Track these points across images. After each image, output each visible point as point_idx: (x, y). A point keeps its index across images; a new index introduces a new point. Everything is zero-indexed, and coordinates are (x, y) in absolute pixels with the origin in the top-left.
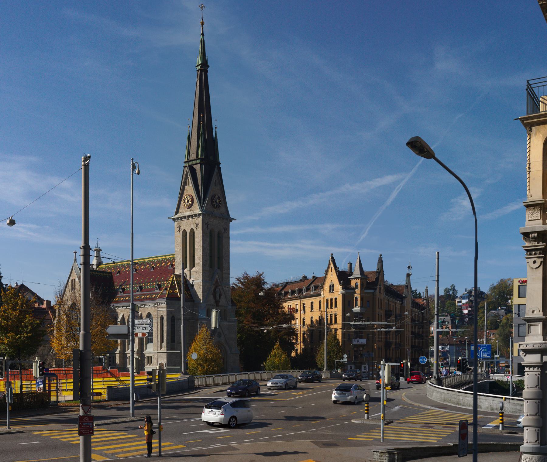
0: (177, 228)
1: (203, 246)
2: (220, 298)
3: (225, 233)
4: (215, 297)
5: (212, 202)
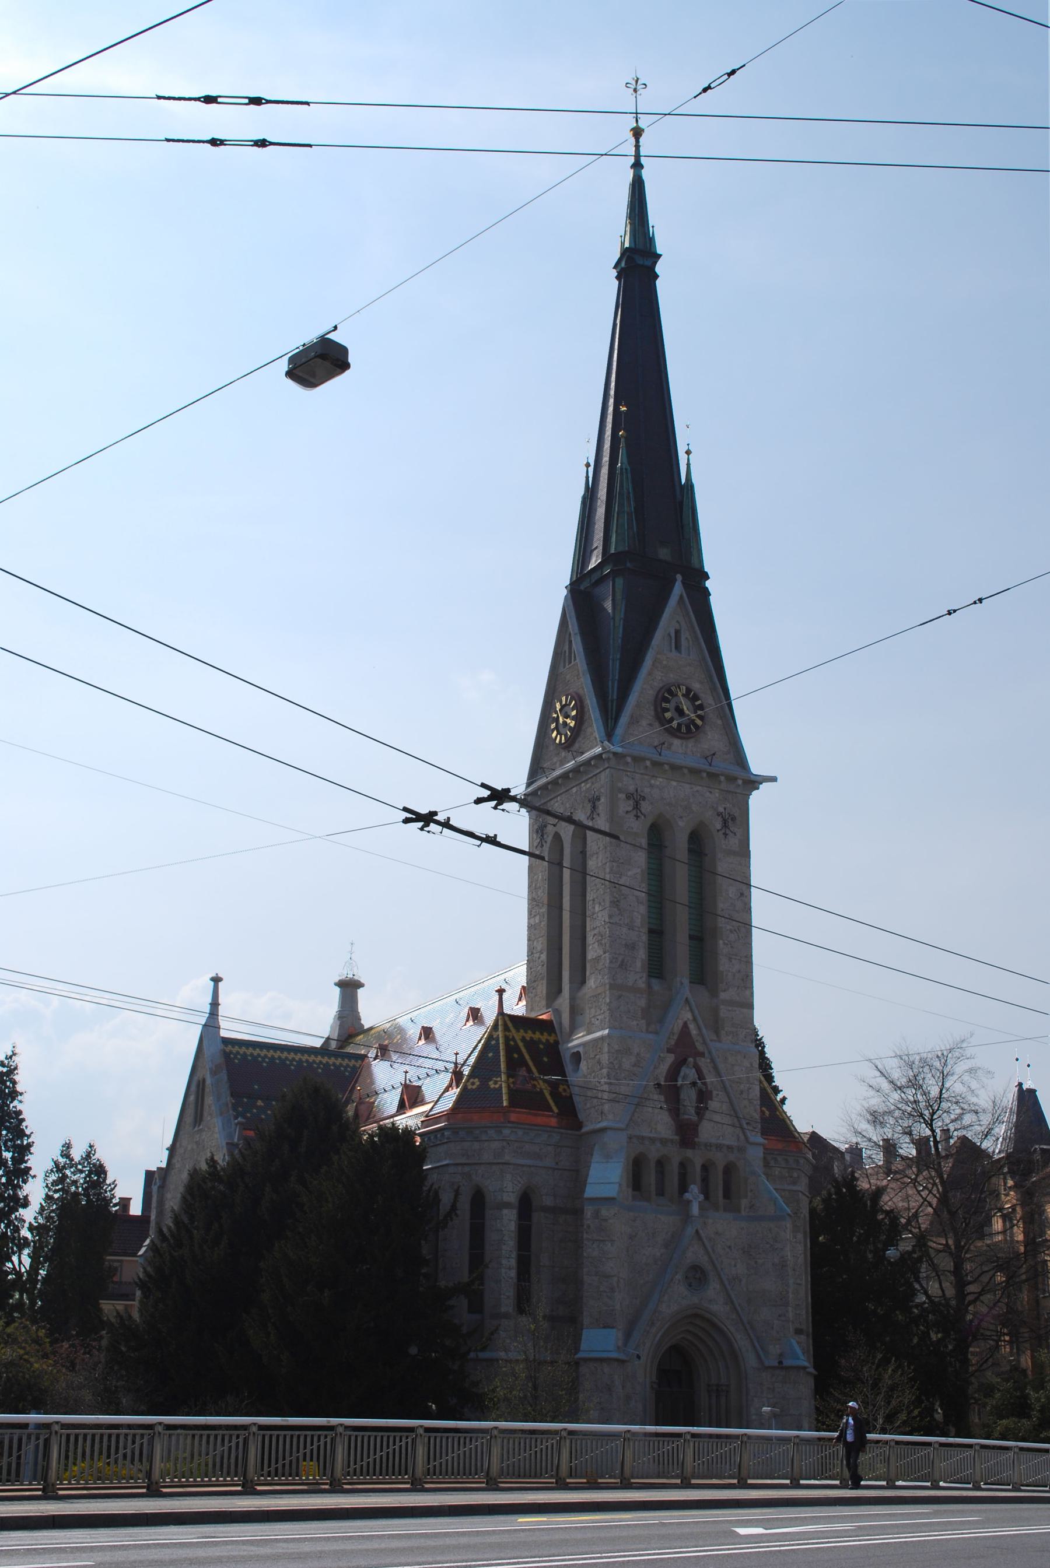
2: (700, 1112)
3: (725, 834)
4: (674, 1106)
5: (659, 710)
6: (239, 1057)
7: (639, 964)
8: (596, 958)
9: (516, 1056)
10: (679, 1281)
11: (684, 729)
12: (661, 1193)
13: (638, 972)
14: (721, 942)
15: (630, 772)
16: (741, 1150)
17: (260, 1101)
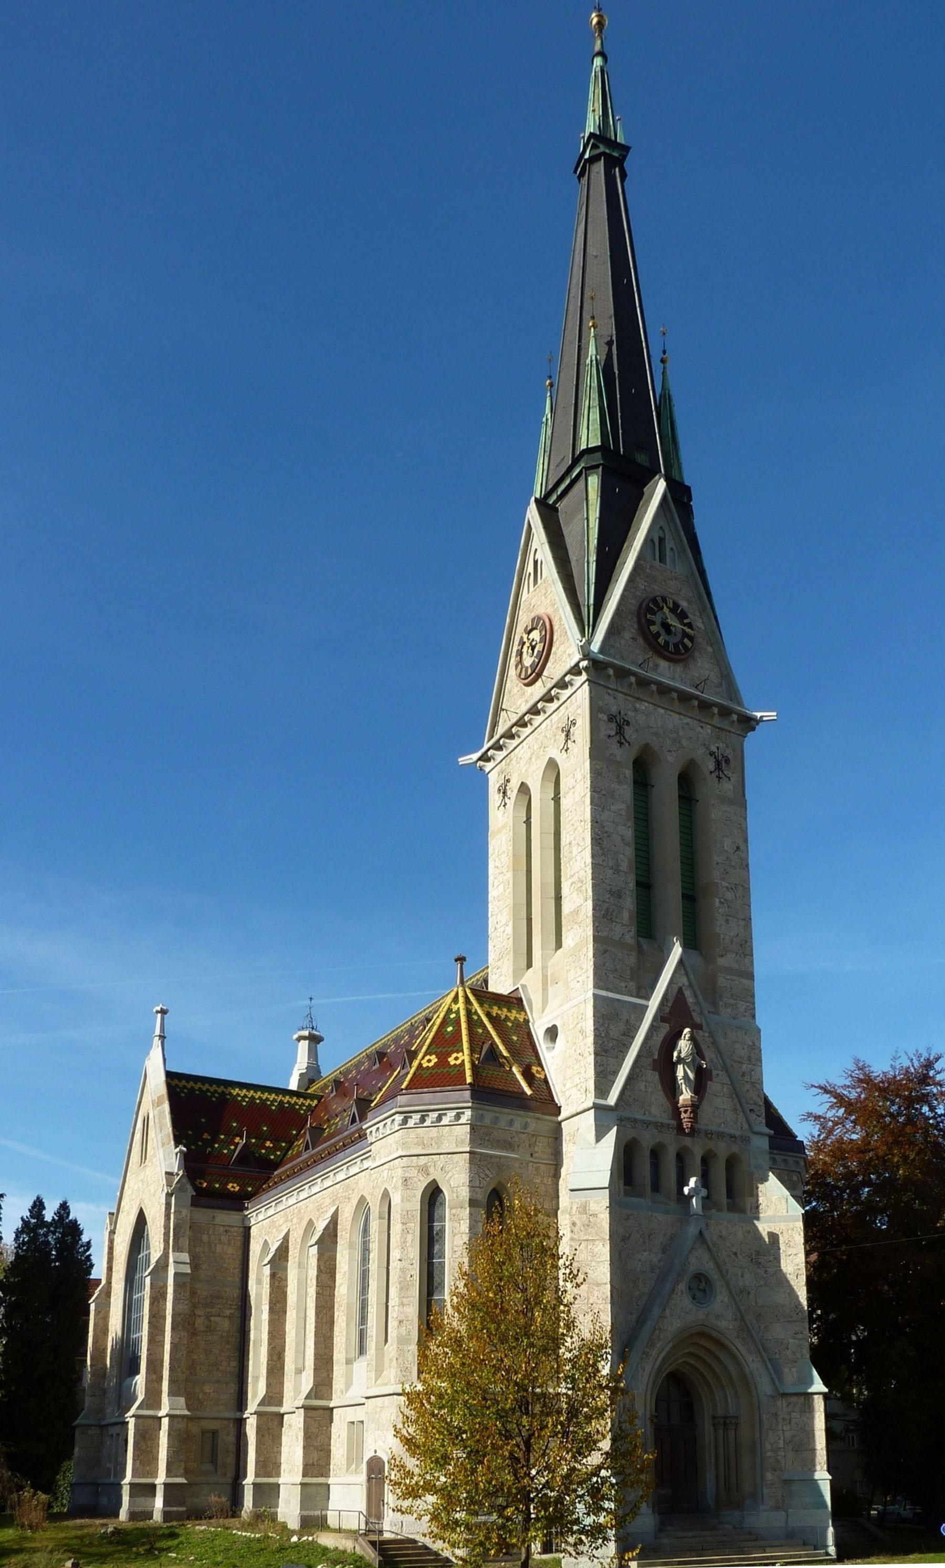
1: (595, 822)
5: (643, 621)
6: (185, 1091)
7: (626, 915)
8: (574, 911)
9: (480, 1031)
10: (682, 1291)
11: (671, 648)
12: (656, 1187)
13: (625, 925)
14: (717, 900)
15: (611, 689)
16: (746, 1140)
17: (206, 1134)
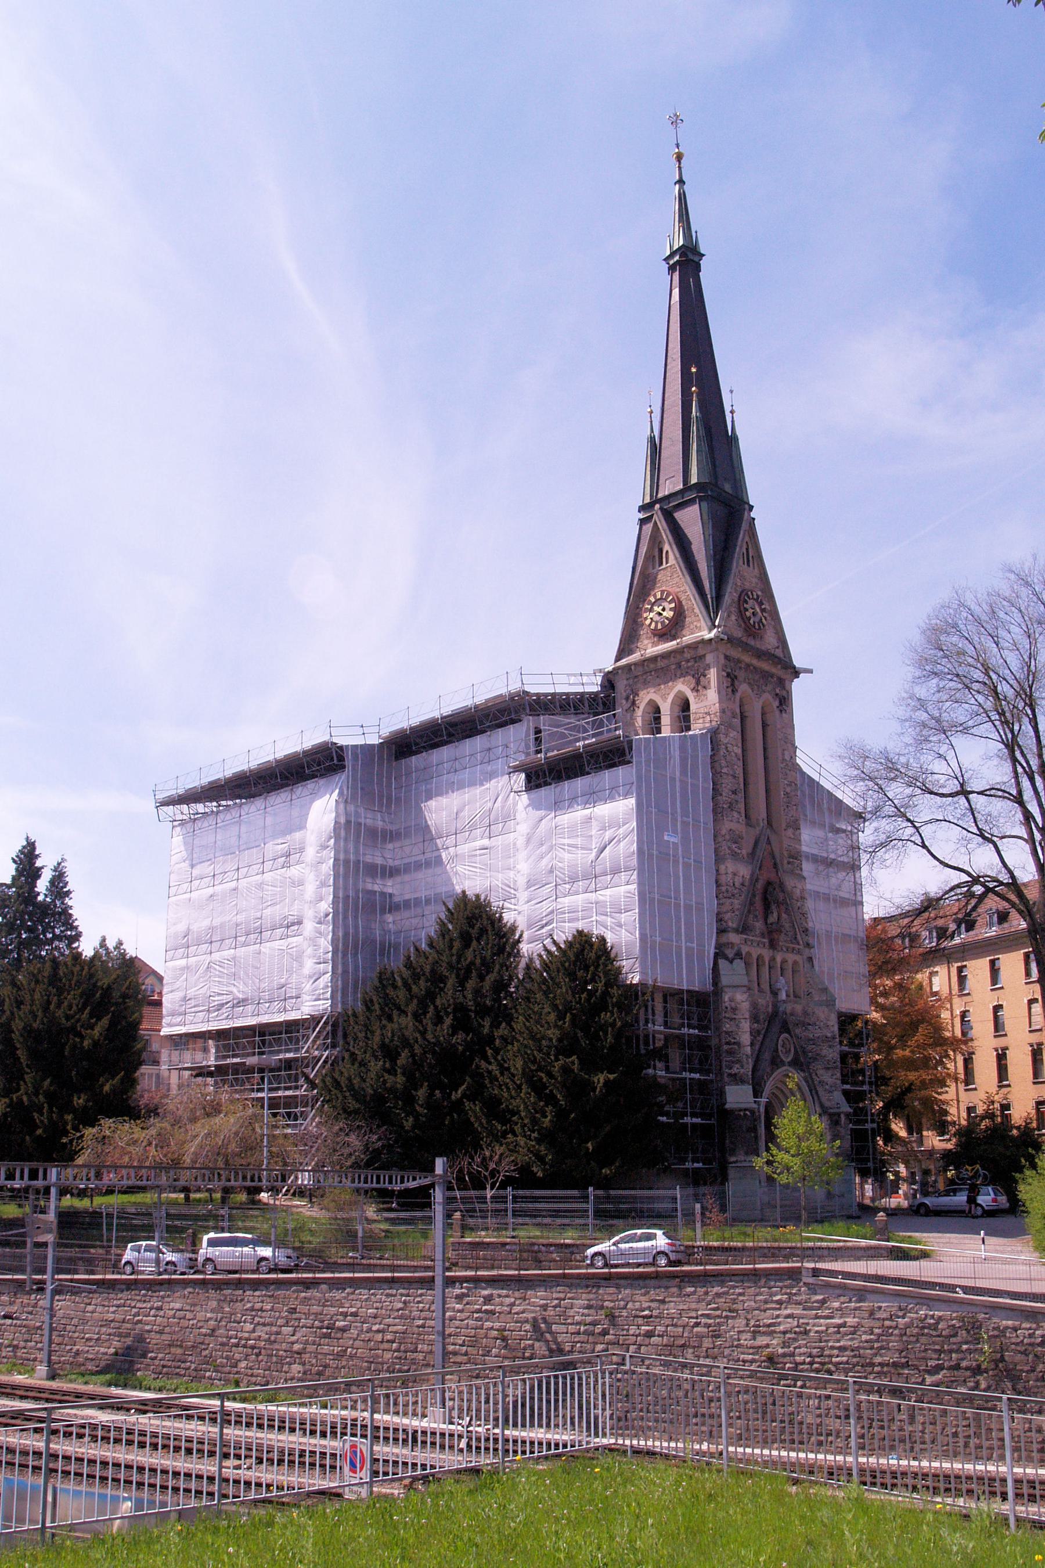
0: (624, 702)
